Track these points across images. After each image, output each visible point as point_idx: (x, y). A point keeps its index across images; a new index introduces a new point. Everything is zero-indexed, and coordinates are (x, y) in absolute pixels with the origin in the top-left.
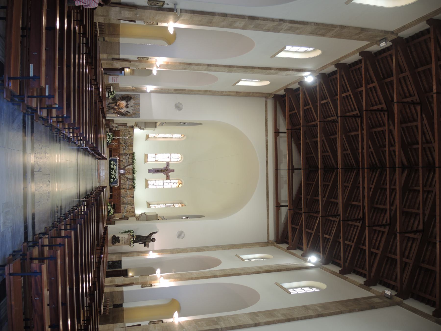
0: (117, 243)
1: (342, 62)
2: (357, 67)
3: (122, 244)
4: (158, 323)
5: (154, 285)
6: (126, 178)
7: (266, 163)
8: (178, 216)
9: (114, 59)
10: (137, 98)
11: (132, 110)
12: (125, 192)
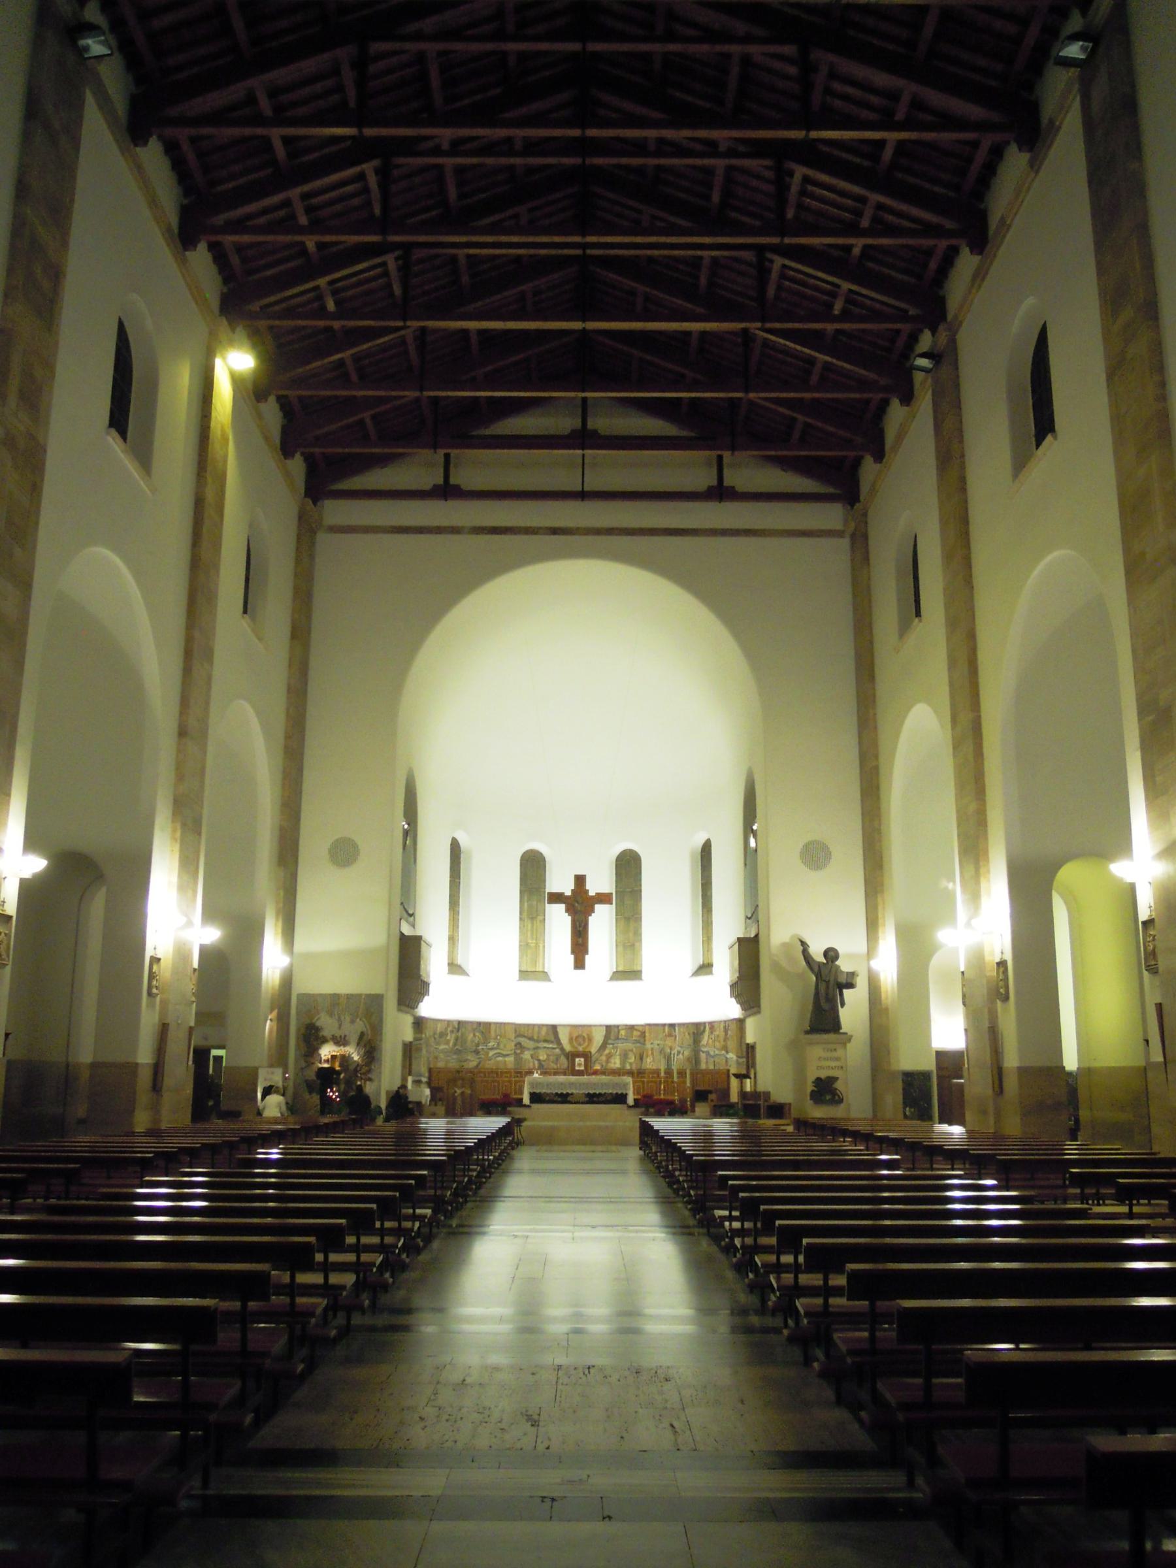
0: (838, 1085)
1: (174, 220)
2: (235, 260)
3: (842, 1067)
4: (1154, 940)
5: (1002, 953)
6: (604, 1050)
7: (559, 534)
8: (745, 865)
9: (156, 1086)
10: (310, 1003)
11: (353, 1022)
12: (652, 1054)
